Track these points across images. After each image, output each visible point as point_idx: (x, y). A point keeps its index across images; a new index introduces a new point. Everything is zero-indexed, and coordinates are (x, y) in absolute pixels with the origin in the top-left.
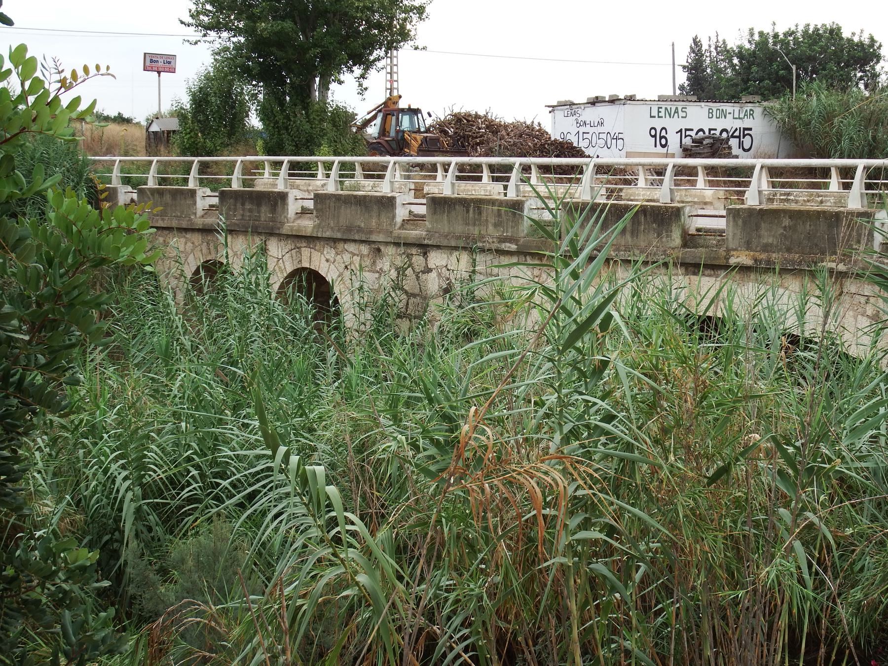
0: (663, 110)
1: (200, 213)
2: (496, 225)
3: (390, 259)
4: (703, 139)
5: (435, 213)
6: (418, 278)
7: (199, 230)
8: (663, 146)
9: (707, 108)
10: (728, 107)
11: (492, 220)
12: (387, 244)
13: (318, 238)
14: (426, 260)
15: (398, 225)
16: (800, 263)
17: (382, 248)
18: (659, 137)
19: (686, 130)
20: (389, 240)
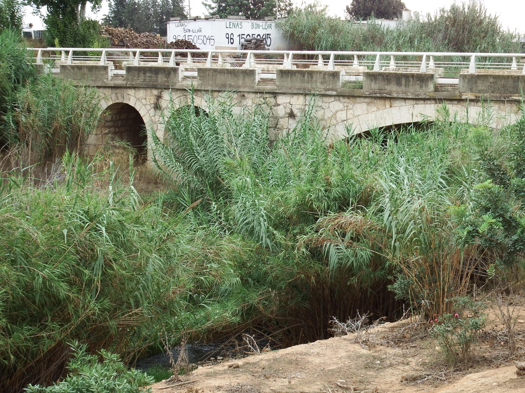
0: (231, 24)
1: (110, 78)
2: (322, 83)
3: (250, 101)
4: (252, 40)
5: (282, 77)
6: (271, 109)
7: (109, 87)
8: (232, 43)
9: (251, 23)
10: (260, 23)
11: (319, 80)
12: (249, 92)
13: (200, 90)
14: (276, 100)
15: (256, 83)
16: (500, 97)
17: (246, 95)
18: (230, 39)
19: (242, 35)
20: (252, 91)
